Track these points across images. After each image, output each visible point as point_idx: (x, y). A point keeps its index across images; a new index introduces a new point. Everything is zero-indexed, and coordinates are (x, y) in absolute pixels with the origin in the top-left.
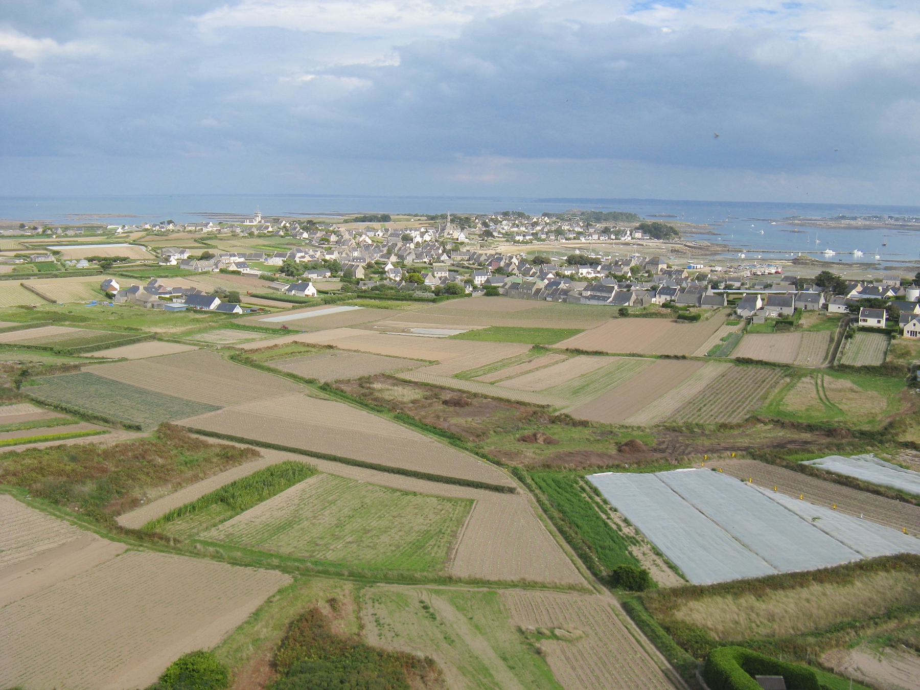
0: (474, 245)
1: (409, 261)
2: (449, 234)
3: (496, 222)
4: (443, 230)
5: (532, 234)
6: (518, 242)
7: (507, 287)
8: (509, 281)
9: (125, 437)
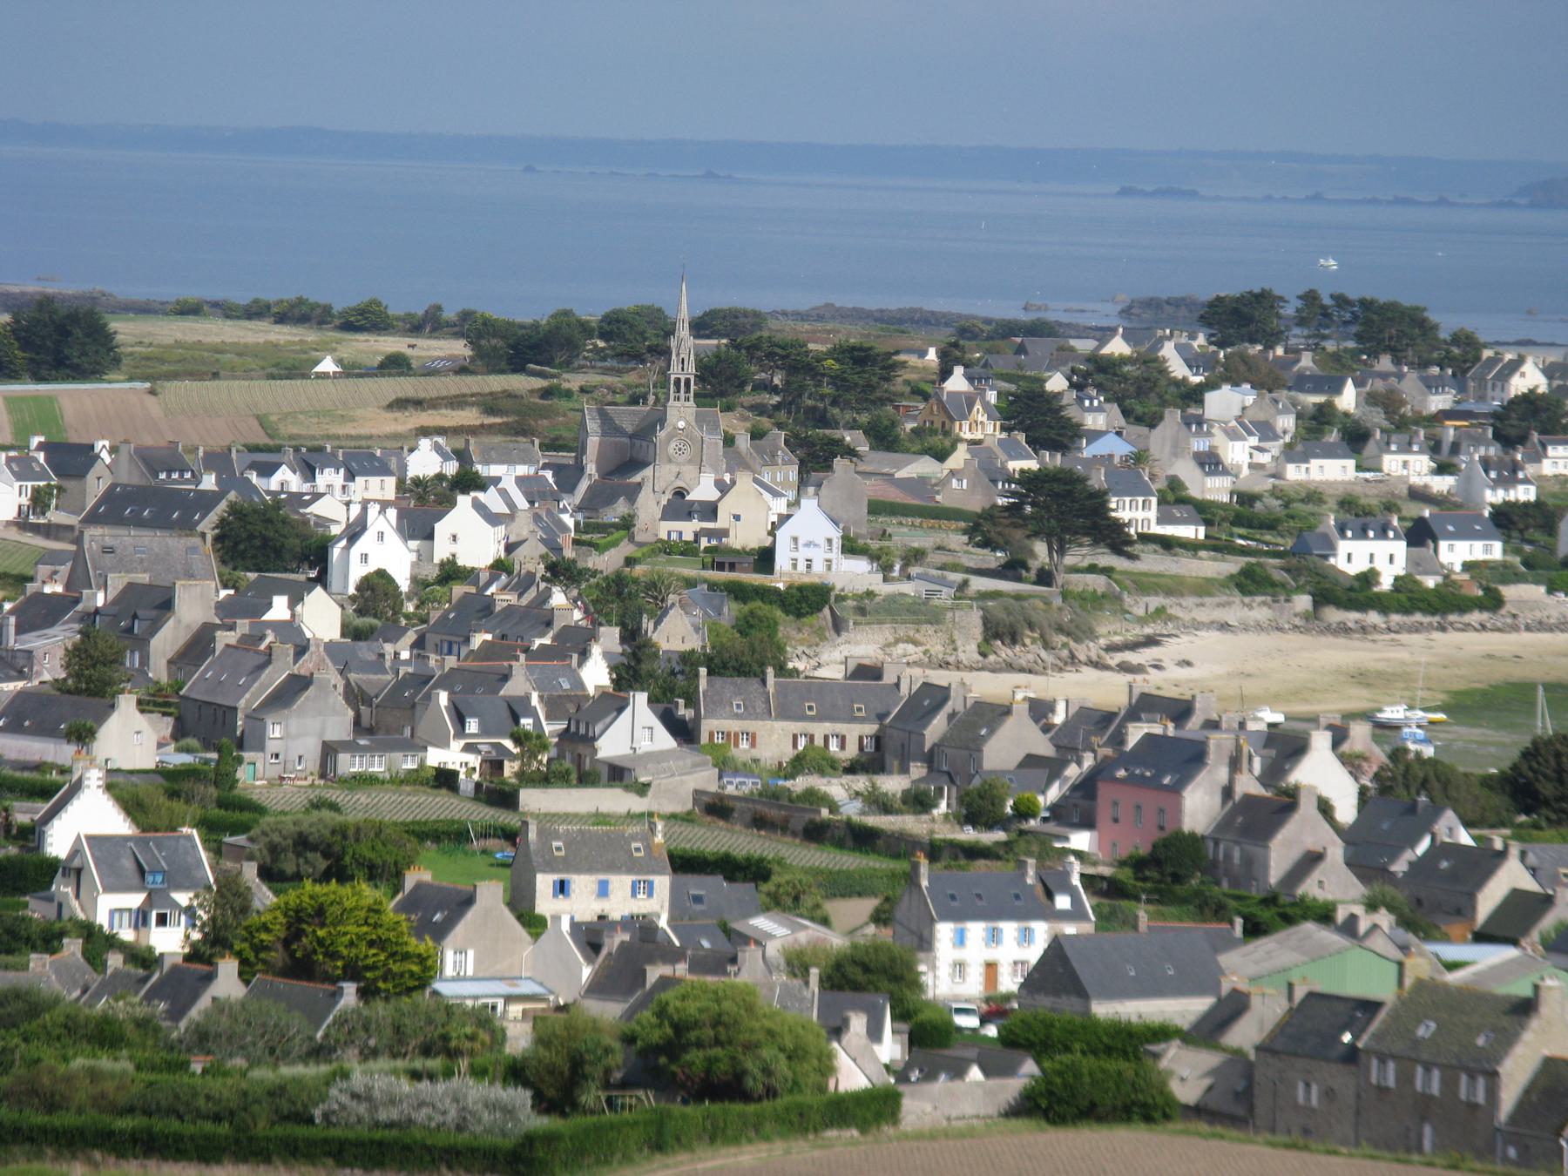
0: (920, 613)
1: (286, 759)
2: (679, 506)
3: (1143, 395)
4: (628, 461)
5: (1505, 520)
6: (1359, 593)
7: (1245, 1035)
8: (1269, 974)
9: (543, 1005)
